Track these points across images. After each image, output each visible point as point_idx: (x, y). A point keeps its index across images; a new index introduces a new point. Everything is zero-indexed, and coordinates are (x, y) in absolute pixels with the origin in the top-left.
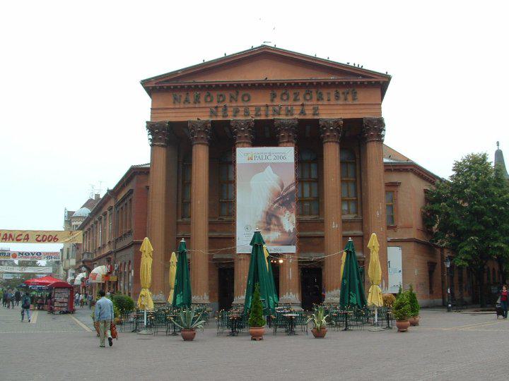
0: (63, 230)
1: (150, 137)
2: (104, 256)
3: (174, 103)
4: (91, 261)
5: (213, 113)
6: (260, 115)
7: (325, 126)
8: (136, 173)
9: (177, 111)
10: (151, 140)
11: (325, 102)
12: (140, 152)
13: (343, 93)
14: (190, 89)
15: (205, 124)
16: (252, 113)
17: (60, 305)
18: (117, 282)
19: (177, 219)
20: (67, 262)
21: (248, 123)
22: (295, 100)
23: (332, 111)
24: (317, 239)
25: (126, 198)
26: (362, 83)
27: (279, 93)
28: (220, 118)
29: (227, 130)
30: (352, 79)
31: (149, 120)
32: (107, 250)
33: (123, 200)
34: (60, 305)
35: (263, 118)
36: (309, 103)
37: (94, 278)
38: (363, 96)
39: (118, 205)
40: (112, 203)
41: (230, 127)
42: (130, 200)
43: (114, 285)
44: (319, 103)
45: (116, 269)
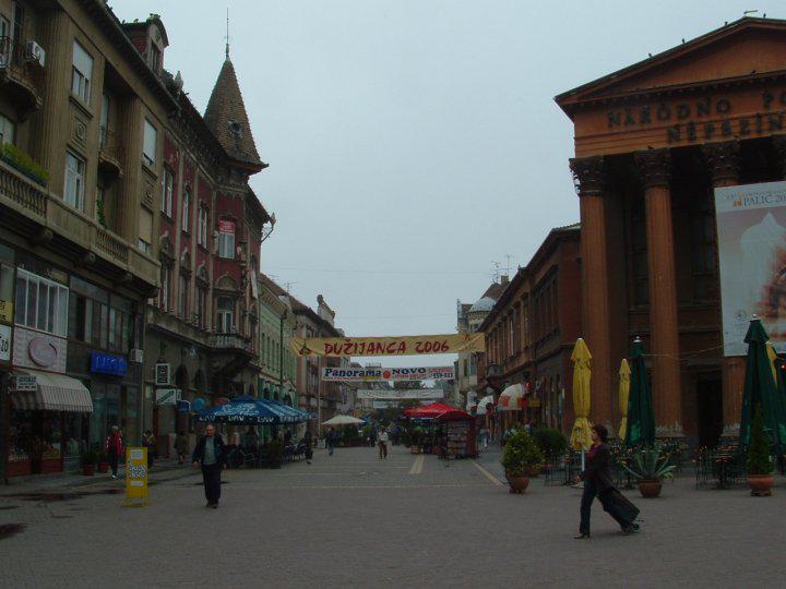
1: (578, 182)
5: (672, 137)
6: (748, 132)
8: (559, 241)
9: (614, 138)
12: (566, 209)
17: (455, 446)
20: (465, 380)
21: (729, 146)
28: (684, 144)
31: (573, 156)
32: (523, 360)
33: (544, 280)
39: (534, 292)
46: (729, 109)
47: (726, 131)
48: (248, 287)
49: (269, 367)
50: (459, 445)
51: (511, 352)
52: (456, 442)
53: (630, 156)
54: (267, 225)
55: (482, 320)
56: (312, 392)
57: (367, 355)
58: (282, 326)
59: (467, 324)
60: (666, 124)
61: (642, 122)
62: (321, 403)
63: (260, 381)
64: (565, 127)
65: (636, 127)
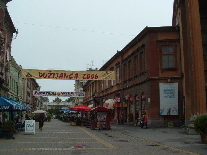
4: (98, 98)
17: (100, 123)
20: (77, 100)
32: (115, 89)
33: (127, 59)
34: (100, 123)
37: (107, 106)
39: (123, 62)
48: (5, 54)
49: (12, 90)
50: (102, 123)
51: (89, 96)
52: (101, 122)
54: (15, 34)
56: (28, 102)
57: (59, 79)
58: (18, 76)
62: (31, 106)
63: (9, 95)
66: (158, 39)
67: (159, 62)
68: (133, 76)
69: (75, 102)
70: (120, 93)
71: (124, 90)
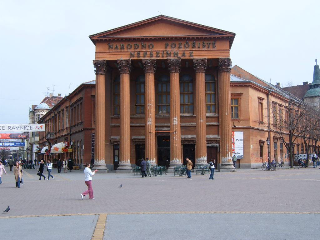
0: (242, 132)
1: (95, 69)
2: (63, 136)
3: (109, 49)
5: (132, 55)
6: (159, 57)
7: (196, 63)
8: (85, 88)
9: (111, 54)
10: (96, 71)
11: (197, 49)
12: (89, 75)
13: (208, 44)
14: (119, 40)
15: (127, 61)
16: (180, 55)
18: (72, 153)
19: (111, 115)
20: (33, 139)
21: (152, 61)
22: (179, 48)
23: (201, 54)
24: (192, 128)
25: (78, 101)
26: (218, 38)
27: (170, 44)
28: (136, 58)
29: (140, 64)
30: (213, 36)
31: (94, 59)
32: (64, 133)
33: (76, 102)
35: (160, 58)
36: (188, 49)
38: (219, 45)
39: (71, 106)
40: (68, 104)
41: (142, 64)
42: (81, 103)
43: (70, 154)
44: (193, 49)
45: (72, 144)
46: (153, 47)
47: (151, 55)
53: (116, 61)
55: (46, 113)
59: (34, 114)
60: (129, 50)
61: (121, 49)
64: (92, 48)
65: (118, 50)
66: (93, 95)
67: (92, 115)
68: (58, 130)
69: (30, 141)
70: (273, 102)
71: (71, 134)
